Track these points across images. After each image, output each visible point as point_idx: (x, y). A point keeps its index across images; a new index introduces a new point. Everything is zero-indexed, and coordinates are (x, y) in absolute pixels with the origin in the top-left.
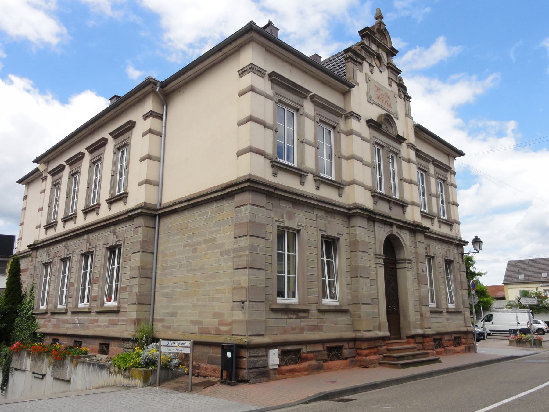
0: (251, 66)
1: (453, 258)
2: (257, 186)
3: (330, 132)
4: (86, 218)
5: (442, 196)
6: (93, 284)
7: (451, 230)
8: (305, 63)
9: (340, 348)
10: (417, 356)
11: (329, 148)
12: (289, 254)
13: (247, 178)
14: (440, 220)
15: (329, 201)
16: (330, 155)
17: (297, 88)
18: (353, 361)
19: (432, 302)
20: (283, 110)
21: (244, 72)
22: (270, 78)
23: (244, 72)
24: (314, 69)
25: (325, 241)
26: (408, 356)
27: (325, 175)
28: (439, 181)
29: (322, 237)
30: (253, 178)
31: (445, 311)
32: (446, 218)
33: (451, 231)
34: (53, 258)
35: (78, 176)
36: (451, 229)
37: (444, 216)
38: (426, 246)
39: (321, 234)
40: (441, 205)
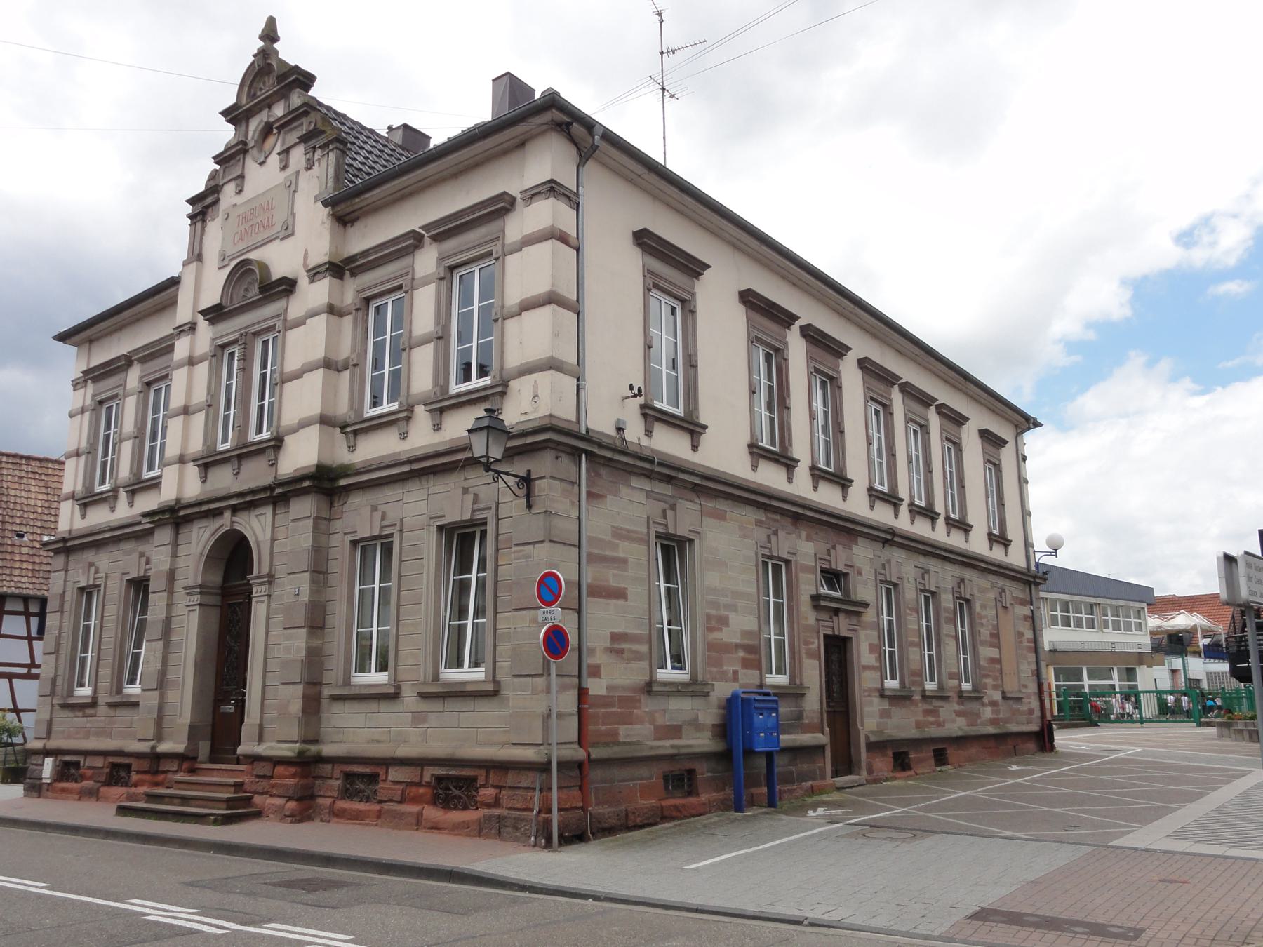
0: (550, 185)
1: (898, 578)
2: (774, 503)
3: (673, 310)
4: (133, 502)
5: (917, 457)
6: (1042, 730)
7: (695, 447)
8: (733, 227)
9: (470, 783)
10: (193, 802)
11: (673, 345)
12: (1128, 681)
13: (546, 422)
14: (874, 493)
15: (785, 496)
16: (674, 360)
17: (677, 255)
18: (488, 818)
19: (893, 678)
20: (658, 302)
21: (533, 195)
22: (637, 240)
23: (533, 195)
24: (788, 263)
25: (662, 545)
26: (172, 797)
27: (663, 405)
28: (912, 427)
29: (657, 537)
30: (555, 422)
31: (917, 697)
32: (885, 489)
33: (844, 500)
34: (189, 614)
35: (117, 404)
36: (843, 496)
37: (954, 512)
38: (959, 580)
39: (656, 532)
40: (822, 437)
